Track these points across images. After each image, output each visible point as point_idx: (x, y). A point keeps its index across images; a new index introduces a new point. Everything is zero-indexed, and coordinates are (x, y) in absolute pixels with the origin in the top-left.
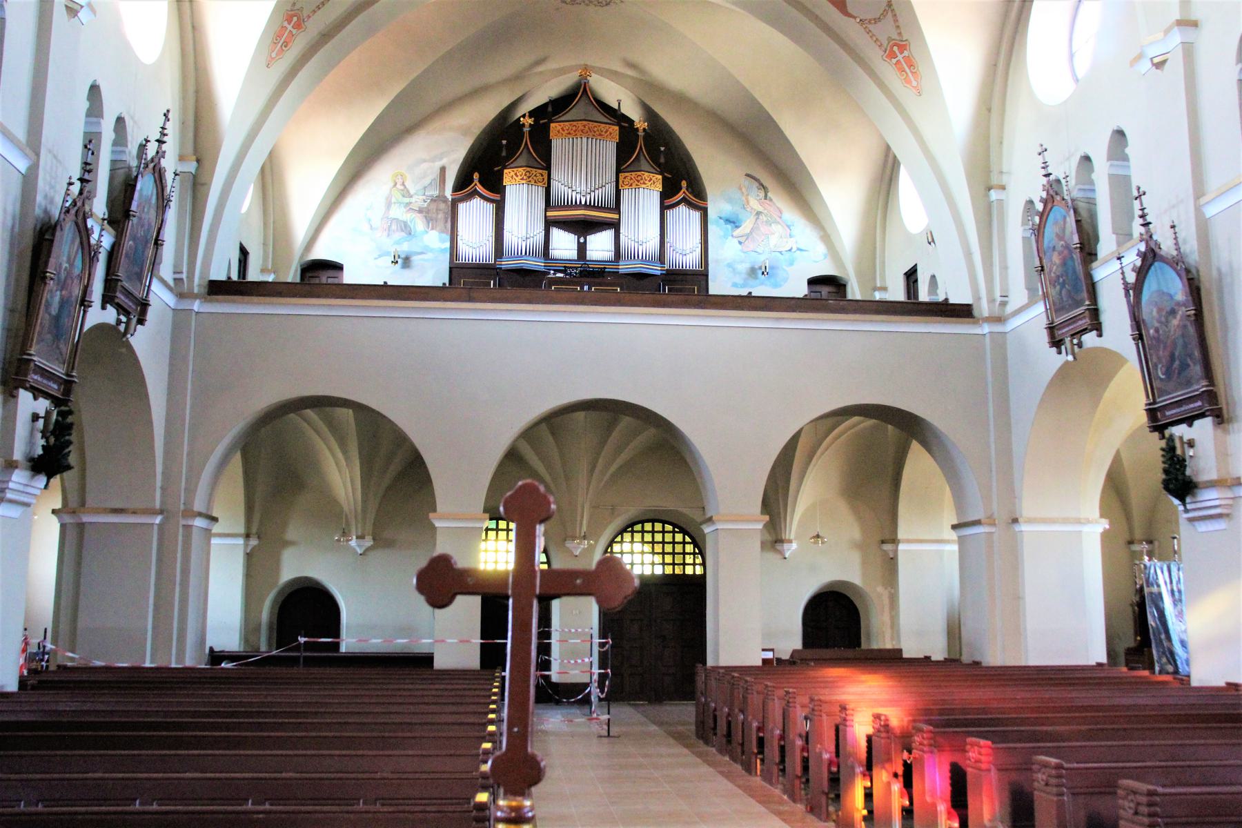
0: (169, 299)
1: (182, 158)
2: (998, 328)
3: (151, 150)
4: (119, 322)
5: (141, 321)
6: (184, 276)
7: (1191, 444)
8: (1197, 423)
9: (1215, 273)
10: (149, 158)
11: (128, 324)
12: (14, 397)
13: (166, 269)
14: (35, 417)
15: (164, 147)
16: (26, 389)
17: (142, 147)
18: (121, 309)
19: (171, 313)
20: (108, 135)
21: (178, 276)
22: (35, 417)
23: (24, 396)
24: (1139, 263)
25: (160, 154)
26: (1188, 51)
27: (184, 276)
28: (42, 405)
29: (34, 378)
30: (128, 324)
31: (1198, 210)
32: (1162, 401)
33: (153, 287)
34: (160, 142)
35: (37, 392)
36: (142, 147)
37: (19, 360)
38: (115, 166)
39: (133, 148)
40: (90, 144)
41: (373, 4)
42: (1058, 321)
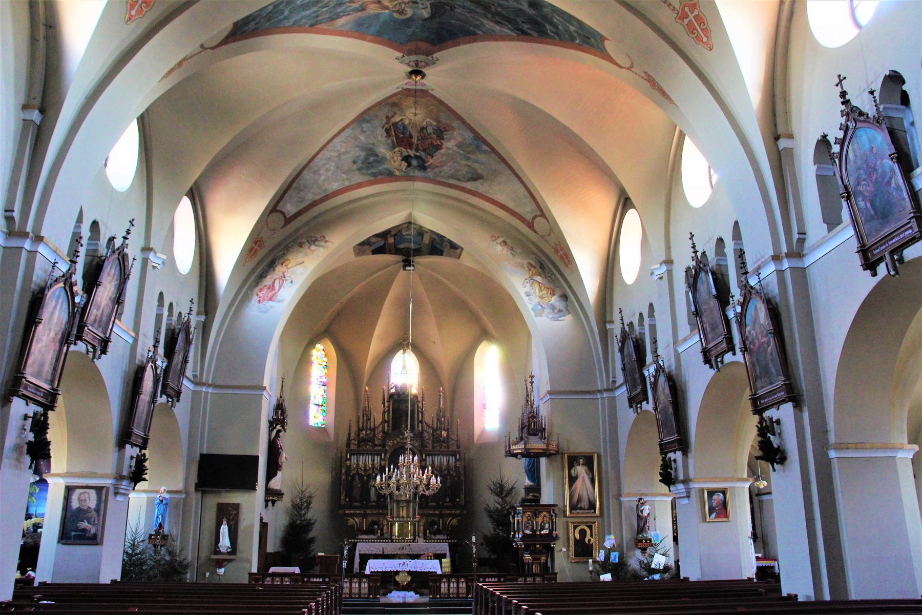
0: (191, 386)
1: (198, 314)
2: (610, 394)
3: (118, 243)
4: (168, 401)
5: (178, 401)
6: (198, 374)
7: (778, 422)
8: (782, 407)
9: (551, 479)
10: (116, 247)
11: (172, 402)
12: (124, 448)
13: (189, 372)
14: (132, 458)
15: (127, 241)
16: (19, 396)
17: (112, 239)
18: (168, 396)
19: (190, 393)
20: (86, 232)
21: (9, 214)
22: (132, 458)
23: (128, 447)
24: (742, 300)
25: (124, 246)
26: (670, 272)
27: (198, 374)
28: (32, 409)
29: (133, 438)
30: (172, 402)
31: (676, 351)
32: (761, 392)
33: (114, 330)
34: (125, 238)
35: (133, 445)
36: (112, 239)
37: (16, 377)
38: (168, 325)
39: (103, 241)
40: (159, 317)
41: (194, 3)
42: (633, 394)
